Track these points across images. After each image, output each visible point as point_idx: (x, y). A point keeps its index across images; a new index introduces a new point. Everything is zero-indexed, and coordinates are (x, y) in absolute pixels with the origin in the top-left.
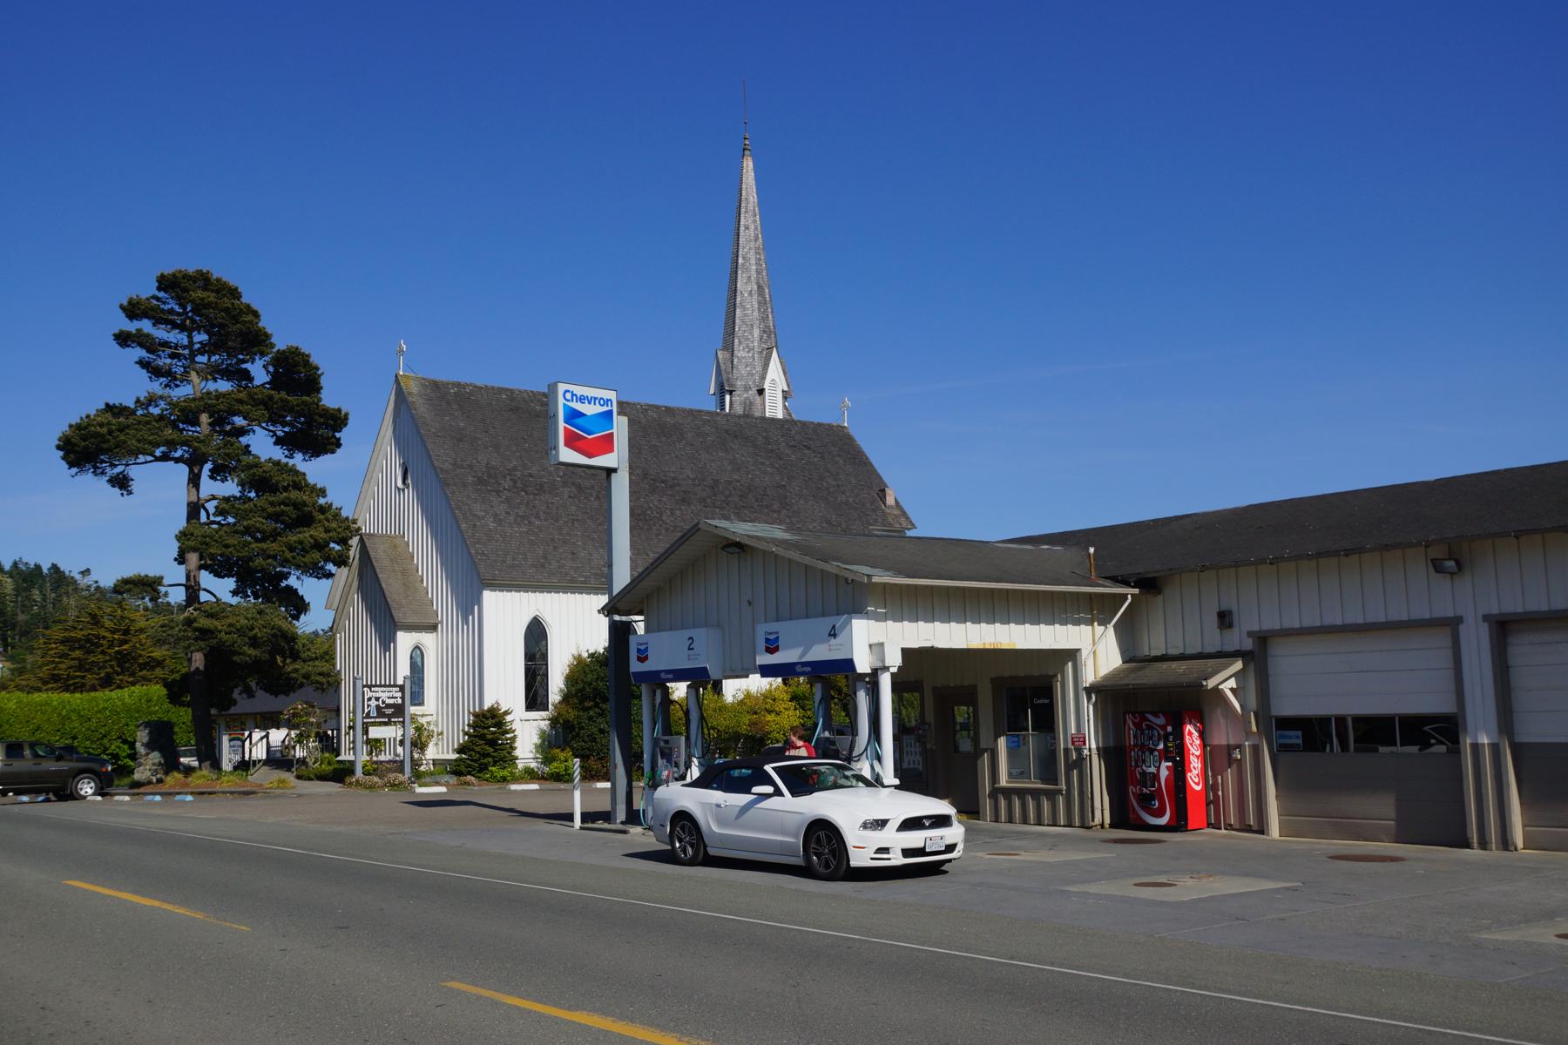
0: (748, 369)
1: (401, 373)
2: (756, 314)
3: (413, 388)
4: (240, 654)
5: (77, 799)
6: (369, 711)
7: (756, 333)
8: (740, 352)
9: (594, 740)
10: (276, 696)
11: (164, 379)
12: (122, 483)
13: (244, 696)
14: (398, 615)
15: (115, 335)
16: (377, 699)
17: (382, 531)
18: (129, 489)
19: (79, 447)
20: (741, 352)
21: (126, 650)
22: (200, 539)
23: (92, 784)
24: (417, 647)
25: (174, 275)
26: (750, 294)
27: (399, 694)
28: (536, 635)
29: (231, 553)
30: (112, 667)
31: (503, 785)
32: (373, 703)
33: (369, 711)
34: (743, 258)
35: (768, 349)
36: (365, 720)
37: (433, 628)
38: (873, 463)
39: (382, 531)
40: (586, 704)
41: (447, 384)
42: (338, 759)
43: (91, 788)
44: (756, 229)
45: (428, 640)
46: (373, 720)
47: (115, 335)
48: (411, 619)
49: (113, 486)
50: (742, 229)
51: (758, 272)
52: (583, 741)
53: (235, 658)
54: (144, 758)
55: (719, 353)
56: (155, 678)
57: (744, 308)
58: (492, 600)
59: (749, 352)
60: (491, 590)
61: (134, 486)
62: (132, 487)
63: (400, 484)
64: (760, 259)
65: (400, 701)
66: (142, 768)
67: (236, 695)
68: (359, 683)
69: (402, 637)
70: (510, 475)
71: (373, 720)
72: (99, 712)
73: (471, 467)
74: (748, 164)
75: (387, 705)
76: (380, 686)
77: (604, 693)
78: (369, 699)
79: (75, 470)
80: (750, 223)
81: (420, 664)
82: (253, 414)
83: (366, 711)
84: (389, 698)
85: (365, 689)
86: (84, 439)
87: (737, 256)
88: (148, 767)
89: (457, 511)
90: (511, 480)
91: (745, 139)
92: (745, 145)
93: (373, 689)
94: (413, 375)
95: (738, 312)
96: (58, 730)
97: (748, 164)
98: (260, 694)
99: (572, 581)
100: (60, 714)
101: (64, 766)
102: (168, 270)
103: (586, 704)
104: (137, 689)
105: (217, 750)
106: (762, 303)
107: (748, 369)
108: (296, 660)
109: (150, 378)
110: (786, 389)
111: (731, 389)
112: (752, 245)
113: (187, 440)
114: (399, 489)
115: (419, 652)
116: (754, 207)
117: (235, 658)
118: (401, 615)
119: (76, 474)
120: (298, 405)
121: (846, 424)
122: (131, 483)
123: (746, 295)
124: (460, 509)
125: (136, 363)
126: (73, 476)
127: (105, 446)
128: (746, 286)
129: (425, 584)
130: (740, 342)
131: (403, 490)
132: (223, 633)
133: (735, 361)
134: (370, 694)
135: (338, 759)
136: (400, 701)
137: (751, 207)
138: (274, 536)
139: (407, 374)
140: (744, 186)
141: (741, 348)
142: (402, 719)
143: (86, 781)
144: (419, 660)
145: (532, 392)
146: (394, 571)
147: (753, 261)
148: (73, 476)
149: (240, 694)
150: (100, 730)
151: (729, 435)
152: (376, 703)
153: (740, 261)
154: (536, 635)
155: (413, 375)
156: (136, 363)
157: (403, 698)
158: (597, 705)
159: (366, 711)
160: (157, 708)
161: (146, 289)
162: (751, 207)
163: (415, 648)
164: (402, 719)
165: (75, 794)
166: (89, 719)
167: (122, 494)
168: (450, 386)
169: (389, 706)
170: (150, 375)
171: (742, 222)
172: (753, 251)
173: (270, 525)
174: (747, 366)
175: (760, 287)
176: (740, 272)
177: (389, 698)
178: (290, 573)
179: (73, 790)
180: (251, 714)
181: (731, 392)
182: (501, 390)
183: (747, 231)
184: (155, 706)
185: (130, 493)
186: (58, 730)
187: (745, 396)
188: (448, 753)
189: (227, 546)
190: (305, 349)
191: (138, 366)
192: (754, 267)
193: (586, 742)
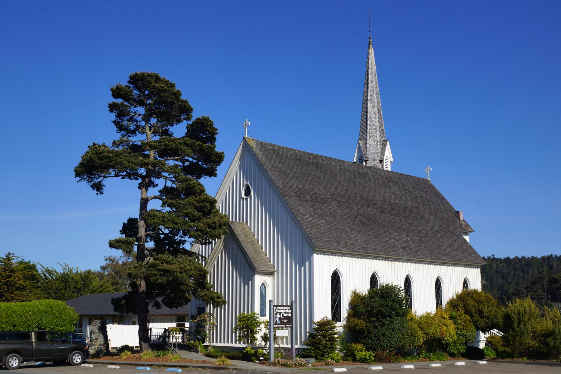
0: (375, 150)
1: (246, 137)
2: (377, 123)
3: (253, 144)
4: (184, 285)
5: (72, 365)
6: (277, 321)
7: (378, 133)
8: (370, 141)
9: (379, 339)
10: (171, 309)
11: (124, 132)
12: (98, 188)
13: (155, 308)
14: (256, 266)
15: (109, 104)
16: (280, 313)
17: (236, 220)
18: (102, 191)
19: (97, 163)
20: (371, 142)
21: (11, 280)
22: (161, 219)
23: (80, 357)
24: (263, 284)
25: (143, 74)
26: (375, 113)
27: (290, 311)
28: (336, 279)
29: (178, 227)
30: (4, 289)
31: (364, 366)
32: (278, 316)
33: (277, 321)
34: (371, 96)
35: (383, 141)
36: (275, 326)
37: (271, 274)
38: (446, 199)
39: (236, 220)
40: (372, 319)
41: (267, 144)
42: (204, 344)
43: (79, 359)
44: (376, 82)
45: (268, 280)
46: (278, 326)
47: (109, 104)
48: (263, 269)
49: (94, 189)
50: (369, 82)
51: (378, 103)
52: (372, 339)
53: (182, 287)
54: (95, 341)
55: (360, 141)
56: (23, 295)
57: (371, 120)
58: (317, 258)
59: (374, 142)
60: (317, 254)
61: (105, 190)
62: (104, 190)
63: (243, 195)
64: (378, 97)
65: (290, 315)
66: (93, 346)
67: (150, 308)
68: (272, 304)
69: (258, 280)
70: (308, 193)
71: (278, 326)
72: (26, 312)
73: (290, 187)
74: (372, 51)
75: (284, 317)
76: (282, 306)
77: (384, 313)
78: (276, 314)
79: (78, 178)
80: (373, 78)
81: (264, 293)
82: (187, 152)
83: (275, 320)
84: (285, 313)
85: (275, 308)
86: (100, 159)
87: (367, 95)
88: (97, 347)
89: (293, 210)
90: (310, 195)
91: (370, 39)
92: (370, 42)
93: (278, 308)
94: (251, 138)
95: (369, 122)
96: (6, 322)
97: (372, 51)
98: (164, 307)
99: (353, 251)
100: (7, 313)
101: (67, 347)
102: (139, 71)
103: (372, 319)
104: (44, 302)
105: (509, 360)
106: (380, 118)
107: (375, 150)
108: (203, 290)
109: (117, 131)
110: (392, 161)
111: (367, 159)
112: (375, 89)
113: (155, 163)
114: (243, 199)
115: (263, 287)
116: (375, 72)
117: (182, 287)
118: (258, 266)
119: (80, 180)
120: (207, 149)
121: (429, 179)
122: (103, 187)
123: (372, 114)
124: (294, 209)
125: (112, 122)
126: (78, 182)
127: (110, 164)
128: (372, 110)
129: (264, 250)
130: (370, 138)
131: (246, 199)
132: (178, 273)
133: (368, 146)
134: (277, 311)
135: (204, 344)
136: (290, 315)
137: (373, 71)
138: (199, 219)
139: (249, 137)
140: (370, 61)
141: (371, 140)
142: (291, 326)
143: (77, 355)
144: (264, 291)
145: (303, 152)
146: (248, 242)
147: (375, 98)
148: (78, 182)
149: (152, 307)
150: (28, 323)
151: (387, 180)
152: (279, 316)
153: (369, 97)
154: (336, 279)
155: (251, 138)
156: (112, 122)
157: (292, 313)
158: (378, 320)
159: (275, 320)
160: (55, 311)
161: (124, 82)
162: (373, 71)
163: (262, 284)
164: (291, 326)
165: (71, 363)
166: (22, 317)
167: (97, 194)
168: (268, 145)
169: (285, 318)
170: (117, 129)
171: (370, 78)
172: (375, 93)
173: (197, 214)
174: (374, 148)
175: (378, 110)
176: (369, 102)
177: (285, 313)
178: (186, 241)
179: (70, 360)
180: (87, 315)
181: (366, 161)
182: (290, 150)
183: (372, 83)
184: (54, 310)
185: (102, 193)
186: (6, 322)
187: (373, 163)
188: (232, 343)
189: (176, 223)
190: (211, 119)
191: (113, 123)
192: (376, 101)
193: (374, 340)
